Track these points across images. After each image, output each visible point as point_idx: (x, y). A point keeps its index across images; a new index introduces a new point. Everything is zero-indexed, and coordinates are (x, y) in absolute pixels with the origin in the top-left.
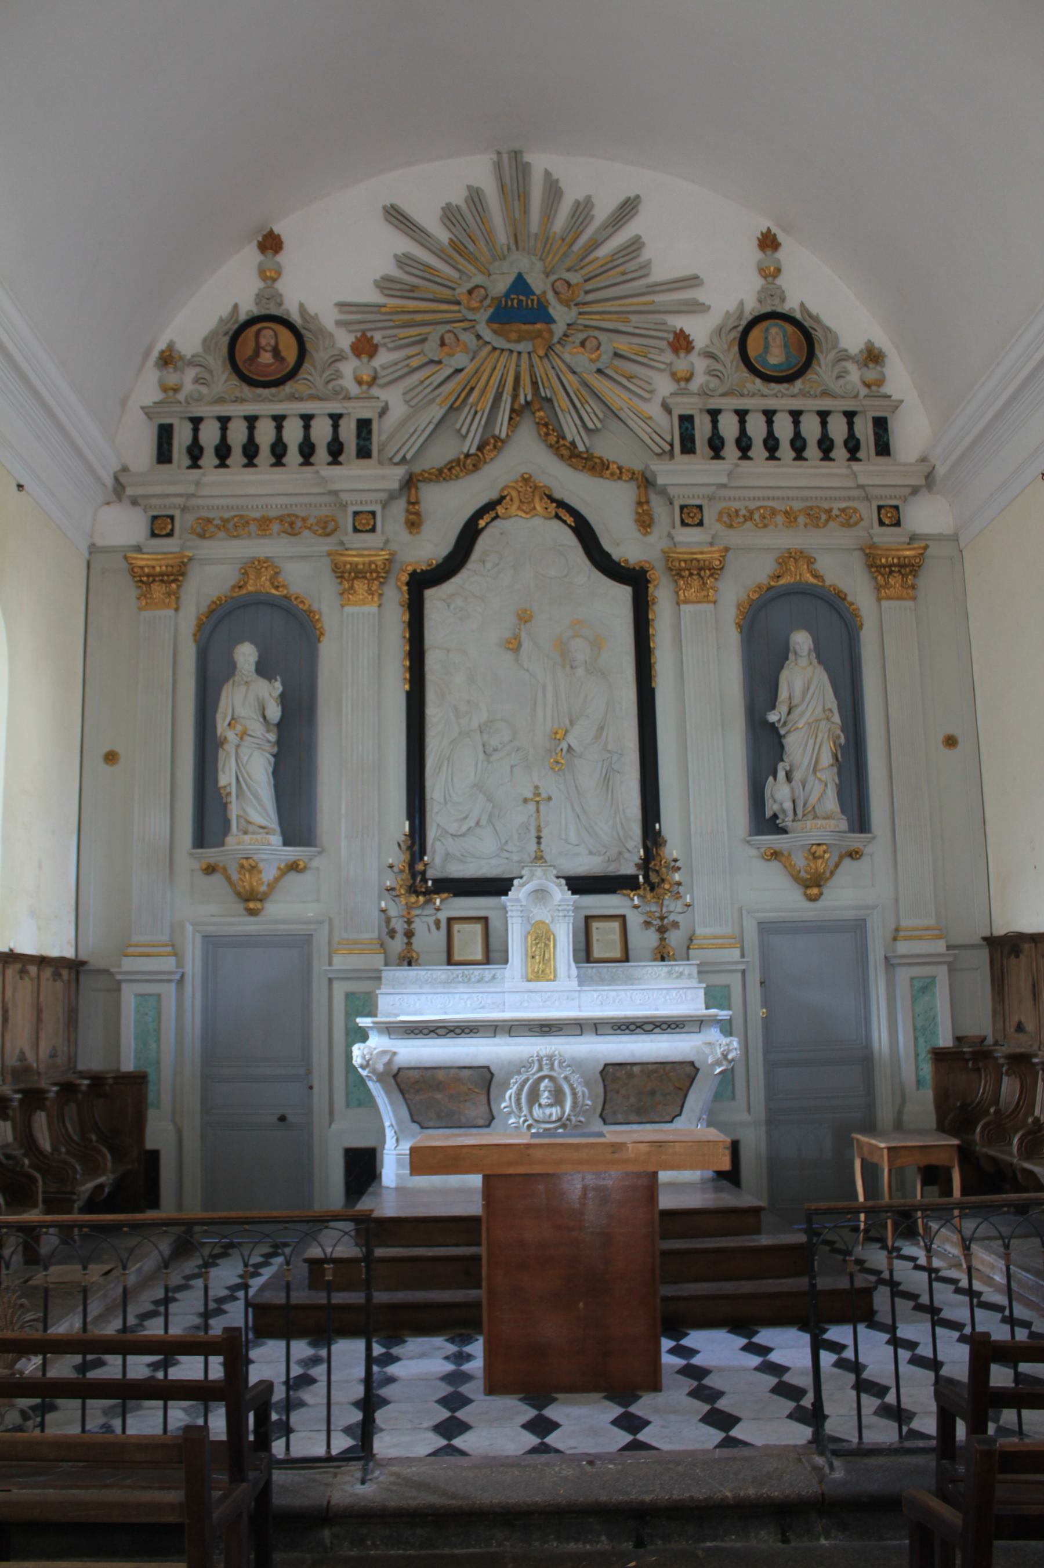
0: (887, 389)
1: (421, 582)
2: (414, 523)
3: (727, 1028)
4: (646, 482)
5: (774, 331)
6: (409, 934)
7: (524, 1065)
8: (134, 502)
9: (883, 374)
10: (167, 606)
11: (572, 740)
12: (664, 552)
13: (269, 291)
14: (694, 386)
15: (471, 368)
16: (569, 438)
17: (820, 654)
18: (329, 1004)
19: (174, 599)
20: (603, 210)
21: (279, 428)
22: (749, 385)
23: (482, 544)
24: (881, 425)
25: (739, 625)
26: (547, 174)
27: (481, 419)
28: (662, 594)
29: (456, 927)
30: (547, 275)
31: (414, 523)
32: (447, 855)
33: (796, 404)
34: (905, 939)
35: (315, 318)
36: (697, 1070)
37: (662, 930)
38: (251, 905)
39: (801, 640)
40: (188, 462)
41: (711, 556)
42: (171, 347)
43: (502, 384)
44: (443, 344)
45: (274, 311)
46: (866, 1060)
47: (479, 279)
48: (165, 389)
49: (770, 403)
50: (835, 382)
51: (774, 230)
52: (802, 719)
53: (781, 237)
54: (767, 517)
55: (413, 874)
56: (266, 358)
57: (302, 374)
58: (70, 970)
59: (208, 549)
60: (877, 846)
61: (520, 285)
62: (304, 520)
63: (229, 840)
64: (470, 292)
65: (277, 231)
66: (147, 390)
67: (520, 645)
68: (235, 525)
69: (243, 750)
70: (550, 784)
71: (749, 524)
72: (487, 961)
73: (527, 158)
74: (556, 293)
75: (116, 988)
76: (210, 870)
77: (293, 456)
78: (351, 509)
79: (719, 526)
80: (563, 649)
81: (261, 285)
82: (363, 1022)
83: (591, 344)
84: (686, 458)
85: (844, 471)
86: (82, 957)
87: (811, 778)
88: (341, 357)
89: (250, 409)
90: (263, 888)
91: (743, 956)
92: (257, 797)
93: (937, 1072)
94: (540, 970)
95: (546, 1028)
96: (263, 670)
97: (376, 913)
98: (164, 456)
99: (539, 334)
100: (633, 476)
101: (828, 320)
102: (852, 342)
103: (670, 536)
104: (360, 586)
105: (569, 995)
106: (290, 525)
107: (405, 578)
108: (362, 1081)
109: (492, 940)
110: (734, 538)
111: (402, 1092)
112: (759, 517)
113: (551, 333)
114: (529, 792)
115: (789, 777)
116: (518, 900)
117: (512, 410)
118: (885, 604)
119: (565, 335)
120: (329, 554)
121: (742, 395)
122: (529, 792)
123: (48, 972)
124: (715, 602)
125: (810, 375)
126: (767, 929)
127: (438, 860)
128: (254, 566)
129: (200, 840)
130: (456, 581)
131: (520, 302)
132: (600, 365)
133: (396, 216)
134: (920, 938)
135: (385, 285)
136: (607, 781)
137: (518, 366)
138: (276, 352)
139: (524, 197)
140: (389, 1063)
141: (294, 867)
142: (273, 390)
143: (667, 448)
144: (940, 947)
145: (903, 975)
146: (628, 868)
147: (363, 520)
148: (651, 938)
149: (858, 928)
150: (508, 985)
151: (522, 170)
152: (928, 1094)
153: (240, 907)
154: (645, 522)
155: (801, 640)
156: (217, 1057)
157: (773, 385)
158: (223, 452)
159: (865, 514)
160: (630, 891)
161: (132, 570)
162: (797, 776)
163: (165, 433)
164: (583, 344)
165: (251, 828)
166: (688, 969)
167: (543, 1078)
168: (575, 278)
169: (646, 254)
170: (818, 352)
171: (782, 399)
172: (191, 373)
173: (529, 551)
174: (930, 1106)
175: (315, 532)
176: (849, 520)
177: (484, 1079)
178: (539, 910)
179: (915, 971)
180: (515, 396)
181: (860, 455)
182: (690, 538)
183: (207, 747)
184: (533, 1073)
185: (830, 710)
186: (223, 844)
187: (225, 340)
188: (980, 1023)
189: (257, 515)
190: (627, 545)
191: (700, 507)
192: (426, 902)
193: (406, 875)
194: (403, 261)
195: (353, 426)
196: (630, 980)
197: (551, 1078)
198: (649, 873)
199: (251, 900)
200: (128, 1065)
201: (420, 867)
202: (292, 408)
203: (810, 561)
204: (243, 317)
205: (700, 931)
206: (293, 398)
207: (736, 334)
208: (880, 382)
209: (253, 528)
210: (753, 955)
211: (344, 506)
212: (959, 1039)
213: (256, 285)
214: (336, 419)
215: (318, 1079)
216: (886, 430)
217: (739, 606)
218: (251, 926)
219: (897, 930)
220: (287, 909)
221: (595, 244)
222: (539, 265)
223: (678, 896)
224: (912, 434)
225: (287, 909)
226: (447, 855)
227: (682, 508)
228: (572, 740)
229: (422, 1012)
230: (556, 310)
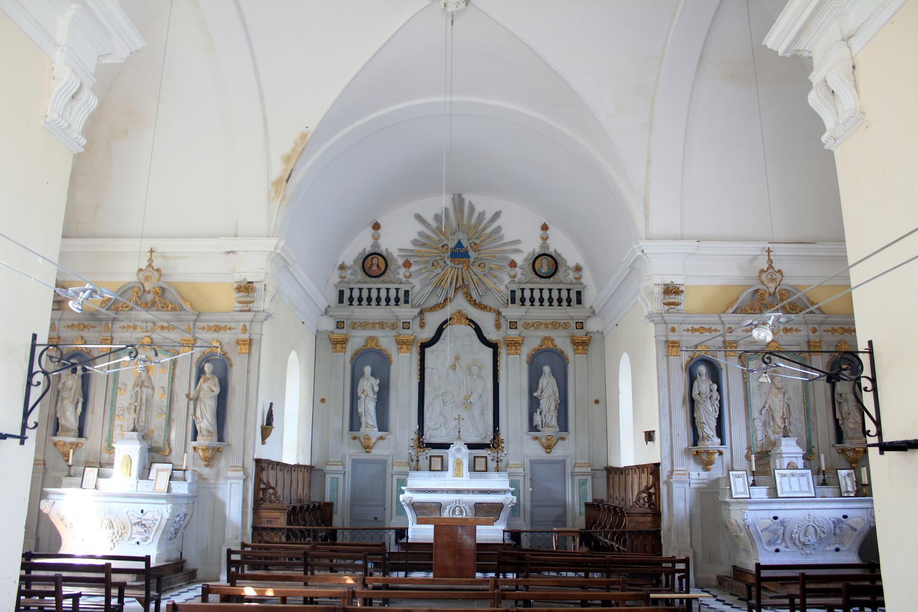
0: (582, 281)
1: (424, 346)
2: (422, 325)
3: (513, 493)
4: (499, 313)
6: (418, 461)
11: (471, 400)
13: (376, 245)
14: (516, 279)
15: (442, 273)
17: (553, 373)
18: (391, 483)
19: (344, 349)
20: (488, 216)
21: (379, 292)
24: (579, 293)
28: (503, 351)
31: (422, 325)
33: (550, 286)
37: (497, 462)
39: (547, 369)
42: (343, 263)
43: (452, 279)
47: (445, 242)
49: (541, 286)
50: (565, 277)
54: (539, 325)
56: (375, 268)
58: (310, 469)
60: (570, 437)
61: (459, 244)
66: (335, 278)
68: (364, 325)
70: (464, 414)
72: (442, 470)
73: (464, 196)
76: (355, 438)
80: (469, 369)
82: (403, 488)
83: (482, 265)
88: (399, 267)
89: (369, 286)
94: (458, 474)
95: (458, 491)
96: (373, 374)
97: (407, 455)
98: (341, 301)
99: (465, 262)
101: (564, 255)
102: (571, 263)
105: (467, 481)
106: (382, 325)
108: (402, 507)
110: (526, 333)
112: (537, 325)
114: (456, 416)
115: (541, 413)
122: (456, 416)
125: (556, 276)
126: (533, 462)
129: (351, 429)
133: (419, 218)
135: (415, 242)
138: (378, 265)
139: (462, 210)
141: (381, 438)
144: (589, 470)
145: (577, 478)
147: (406, 325)
148: (495, 464)
149: (563, 463)
152: (583, 518)
154: (498, 326)
155: (547, 369)
156: (355, 501)
158: (360, 300)
163: (341, 293)
168: (477, 242)
169: (503, 232)
171: (546, 284)
172: (350, 271)
173: (459, 334)
176: (566, 326)
177: (439, 506)
178: (458, 454)
179: (581, 477)
180: (456, 283)
182: (513, 333)
183: (354, 399)
184: (454, 505)
187: (361, 261)
188: (602, 495)
190: (492, 334)
194: (421, 234)
196: (486, 478)
198: (495, 443)
199: (367, 448)
200: (327, 500)
203: (552, 340)
206: (384, 282)
207: (532, 261)
208: (579, 278)
210: (528, 471)
211: (399, 320)
213: (371, 241)
214: (397, 290)
215: (388, 506)
218: (366, 456)
220: (379, 451)
221: (485, 228)
223: (503, 451)
224: (589, 297)
225: (379, 451)
228: (471, 400)
229: (421, 486)
230: (471, 253)
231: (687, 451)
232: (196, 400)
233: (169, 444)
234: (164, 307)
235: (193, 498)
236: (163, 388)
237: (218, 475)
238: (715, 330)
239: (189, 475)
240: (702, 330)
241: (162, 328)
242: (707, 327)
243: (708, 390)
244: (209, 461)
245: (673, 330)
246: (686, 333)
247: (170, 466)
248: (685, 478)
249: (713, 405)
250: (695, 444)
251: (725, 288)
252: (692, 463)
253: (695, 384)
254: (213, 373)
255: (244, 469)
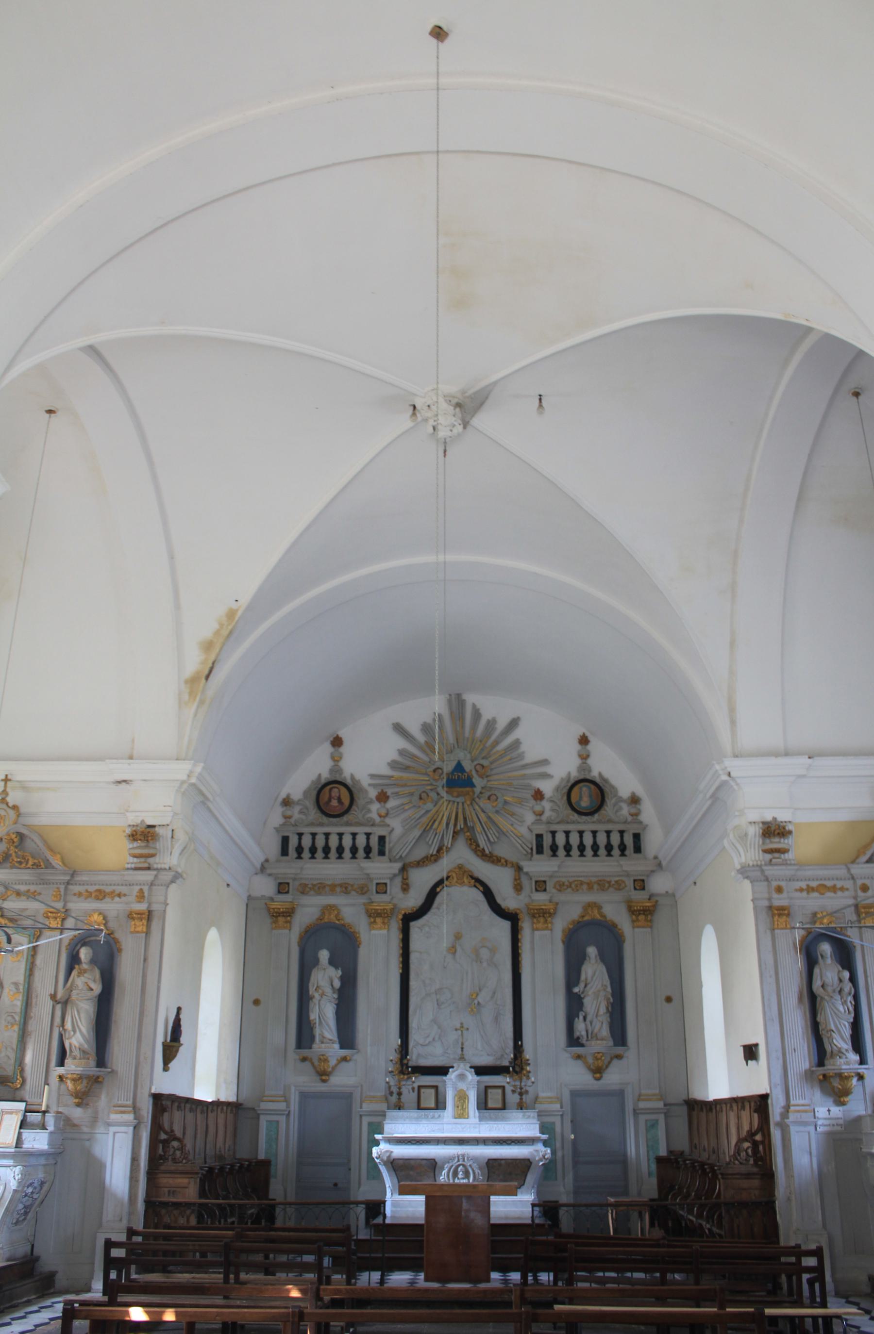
1: (408, 919)
2: (406, 887)
3: (546, 1143)
4: (519, 869)
5: (584, 789)
6: (400, 1094)
7: (450, 1159)
8: (270, 875)
9: (639, 810)
10: (285, 928)
11: (480, 999)
12: (526, 905)
14: (544, 818)
15: (434, 810)
16: (481, 847)
17: (602, 957)
20: (501, 725)
22: (571, 817)
23: (438, 900)
24: (637, 837)
25: (563, 942)
26: (474, 705)
27: (438, 837)
29: (422, 1090)
30: (472, 761)
31: (406, 887)
32: (419, 1055)
33: (594, 827)
34: (643, 1100)
35: (358, 782)
36: (531, 1163)
37: (521, 1094)
38: (324, 1078)
39: (592, 951)
40: (295, 855)
41: (551, 907)
43: (449, 819)
44: (421, 798)
45: (339, 779)
46: (624, 1161)
48: (286, 817)
49: (581, 827)
51: (587, 734)
52: (591, 991)
53: (591, 738)
54: (579, 885)
55: (402, 1064)
56: (334, 803)
57: (352, 812)
58: (234, 1107)
59: (307, 900)
60: (631, 1054)
61: (459, 767)
62: (352, 886)
63: (314, 1046)
64: (435, 771)
65: (340, 736)
66: (276, 819)
67: (456, 951)
68: (320, 888)
69: (322, 1002)
71: (569, 890)
72: (437, 1107)
74: (477, 771)
75: (258, 1117)
76: (304, 1059)
77: (347, 854)
78: (375, 882)
79: (554, 891)
80: (476, 952)
81: (332, 763)
82: (378, 1137)
84: (539, 856)
85: (616, 863)
86: (240, 1101)
87: (595, 1020)
88: (371, 802)
89: (327, 830)
90: (330, 1069)
91: (562, 1107)
92: (328, 1025)
93: (658, 1168)
94: (461, 1113)
95: (461, 1141)
96: (332, 962)
97: (384, 1083)
98: (284, 851)
99: (468, 793)
100: (513, 865)
101: (614, 781)
102: (624, 792)
103: (530, 897)
104: (379, 920)
105: (474, 1126)
106: (345, 888)
107: (401, 917)
108: (376, 1166)
109: (440, 1097)
110: (561, 897)
111: (395, 1170)
112: (576, 885)
113: (474, 793)
114: (456, 1027)
115: (585, 1018)
116: (451, 1079)
117: (454, 832)
118: (636, 930)
119: (481, 793)
120: (364, 904)
121: (568, 823)
122: (456, 1027)
123: (229, 1108)
124: (551, 930)
125: (602, 812)
126: (575, 1094)
127: (414, 1057)
128: (329, 908)
129: (300, 1045)
130: (426, 918)
131: (459, 776)
132: (497, 809)
133: (399, 729)
134: (650, 1100)
135: (393, 765)
136: (497, 1019)
137: (457, 808)
138: (339, 800)
140: (389, 1156)
141: (344, 1059)
142: (338, 819)
143: (529, 851)
144: (660, 1105)
145: (642, 1118)
146: (506, 1063)
150: (445, 1120)
151: (461, 703)
152: (654, 1181)
153: (318, 1078)
154: (518, 888)
155: (592, 951)
157: (583, 817)
158: (313, 850)
159: (627, 883)
160: (504, 1077)
161: (268, 909)
162: (589, 1018)
163: (285, 840)
164: (489, 798)
165: (325, 1041)
166: (532, 1114)
167: (459, 1165)
170: (606, 799)
171: (587, 825)
172: (297, 809)
173: (460, 905)
174: (655, 1187)
175: (357, 892)
176: (619, 886)
177: (432, 1165)
178: (461, 1083)
180: (455, 825)
181: (627, 853)
184: (455, 1163)
185: (606, 986)
186: (311, 1048)
187: (315, 793)
188: (682, 1144)
189: (329, 883)
190: (509, 900)
191: (545, 882)
192: (408, 1078)
193: (398, 1066)
195: (376, 839)
196: (504, 1119)
197: (464, 1165)
198: (516, 1066)
200: (262, 1156)
201: (405, 1061)
202: (347, 830)
203: (599, 908)
204: (323, 781)
205: (541, 1095)
206: (348, 824)
207: (566, 790)
209: (327, 889)
210: (568, 1108)
212: (670, 1152)
214: (368, 835)
215: (354, 1165)
216: (639, 840)
217: (563, 931)
219: (640, 1095)
220: (341, 1080)
221: (496, 743)
222: (469, 756)
223: (528, 1078)
224: (653, 841)
226: (419, 1055)
227: (536, 882)
228: (480, 999)
229: (406, 1133)
230: (477, 780)
231: (809, 1076)
232: (65, 1003)
233: (22, 1071)
234: (22, 863)
235: (55, 1156)
236: (16, 984)
237: (95, 1120)
238: (842, 889)
239: (50, 1119)
240: (822, 889)
241: (18, 894)
242: (829, 884)
243: (836, 979)
244: (83, 1098)
245: (779, 890)
246: (798, 894)
247: (22, 1106)
248: (809, 1117)
249: (844, 1003)
250: (821, 1063)
251: (852, 825)
252: (818, 1094)
253: (816, 971)
254: (93, 961)
255: (135, 1109)
